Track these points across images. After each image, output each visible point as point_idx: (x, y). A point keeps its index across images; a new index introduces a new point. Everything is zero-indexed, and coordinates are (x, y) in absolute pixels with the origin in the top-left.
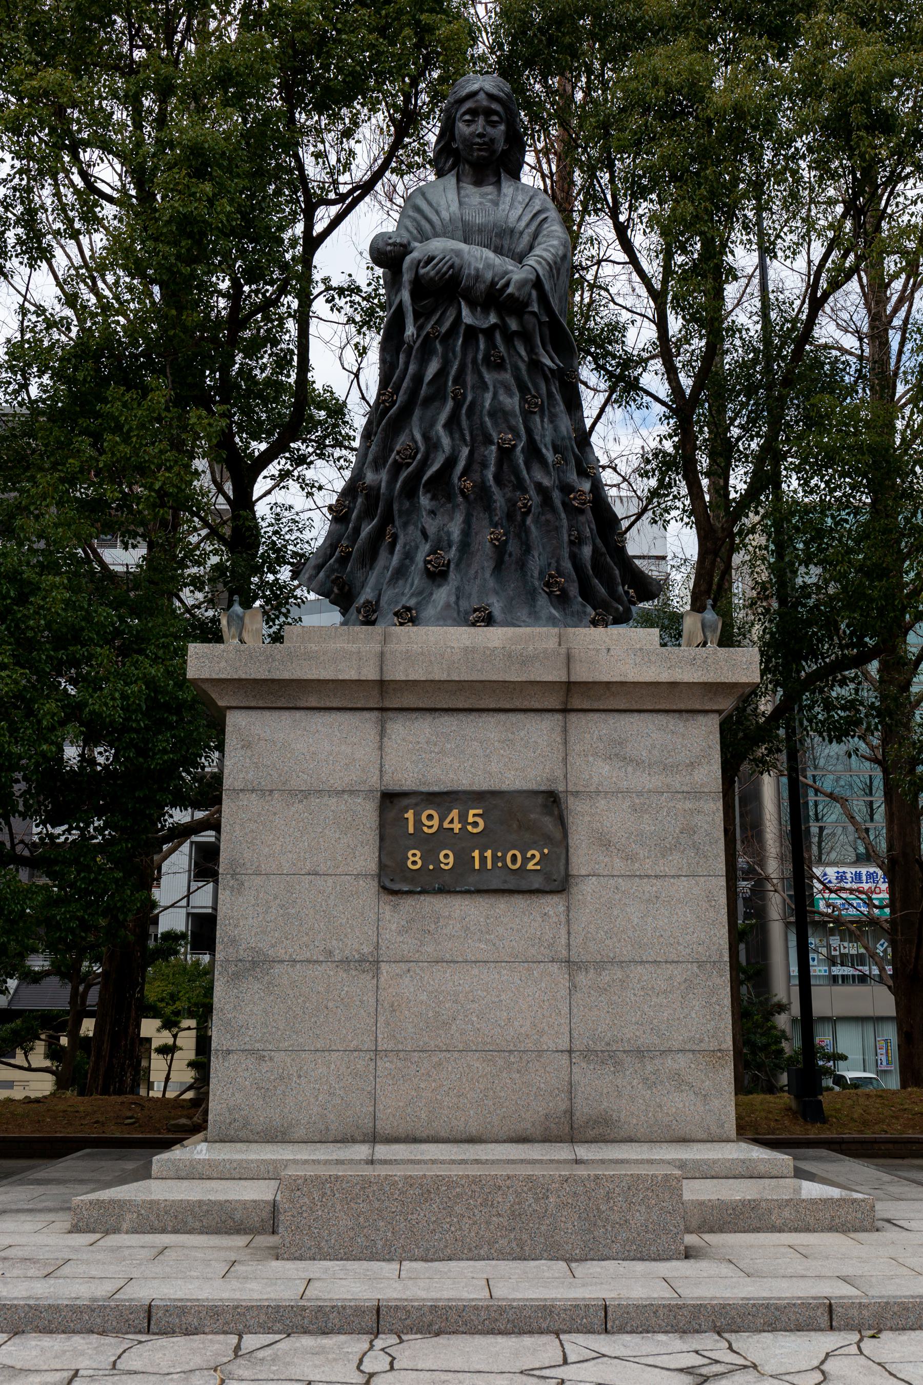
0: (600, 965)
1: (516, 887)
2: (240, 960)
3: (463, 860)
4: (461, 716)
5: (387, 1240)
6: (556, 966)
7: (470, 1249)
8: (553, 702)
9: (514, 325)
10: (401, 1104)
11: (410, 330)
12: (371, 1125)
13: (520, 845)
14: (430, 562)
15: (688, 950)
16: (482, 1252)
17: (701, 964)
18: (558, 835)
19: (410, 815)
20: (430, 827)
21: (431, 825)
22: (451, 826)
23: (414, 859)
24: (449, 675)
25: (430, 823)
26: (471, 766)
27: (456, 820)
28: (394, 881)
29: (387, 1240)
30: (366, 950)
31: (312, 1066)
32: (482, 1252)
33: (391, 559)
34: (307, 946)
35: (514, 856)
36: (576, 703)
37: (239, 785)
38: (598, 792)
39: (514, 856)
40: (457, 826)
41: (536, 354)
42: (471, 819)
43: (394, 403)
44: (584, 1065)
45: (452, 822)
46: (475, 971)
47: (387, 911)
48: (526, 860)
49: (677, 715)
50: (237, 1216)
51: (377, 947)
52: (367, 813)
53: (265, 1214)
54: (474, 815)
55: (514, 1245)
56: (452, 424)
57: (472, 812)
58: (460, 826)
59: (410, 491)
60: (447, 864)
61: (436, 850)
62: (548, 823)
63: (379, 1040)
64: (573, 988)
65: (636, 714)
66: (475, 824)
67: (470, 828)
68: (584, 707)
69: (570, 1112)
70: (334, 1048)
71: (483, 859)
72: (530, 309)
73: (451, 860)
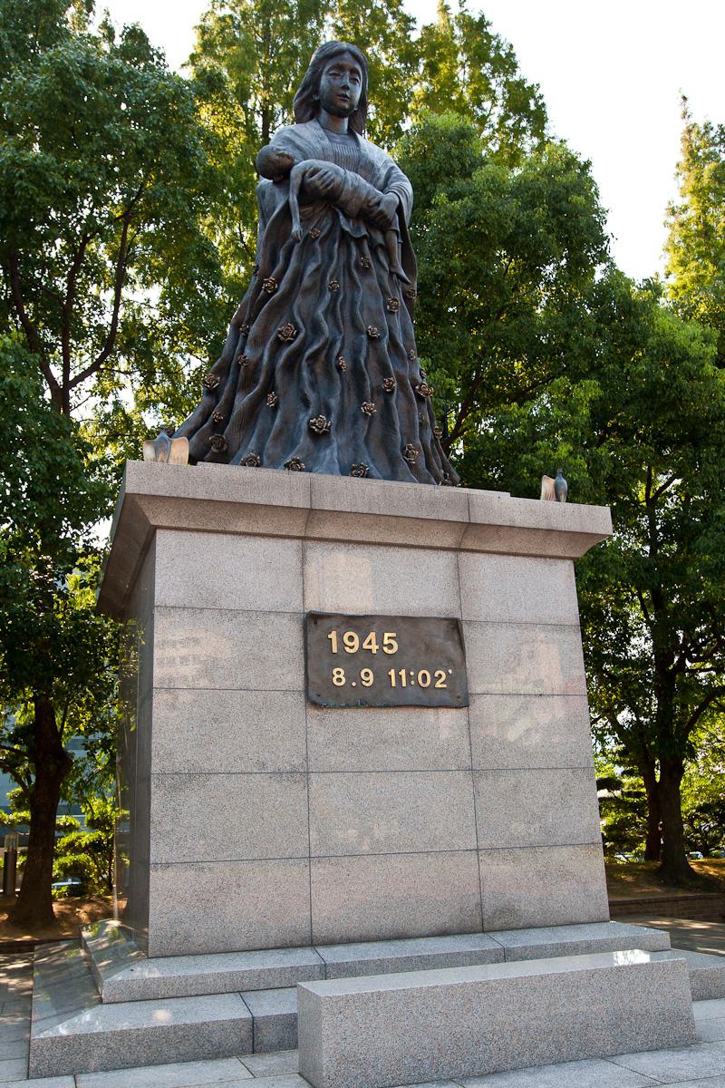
0: (497, 771)
1: (427, 701)
2: (176, 773)
3: (382, 678)
4: (371, 549)
5: (434, 1058)
6: (462, 774)
7: (513, 1057)
8: (448, 541)
9: (379, 239)
10: (335, 907)
11: (296, 228)
12: (308, 929)
13: (422, 664)
14: (314, 424)
15: (564, 759)
16: (525, 1059)
17: (574, 770)
18: (459, 660)
19: (333, 636)
20: (352, 647)
21: (353, 646)
22: (369, 647)
23: (339, 676)
24: (370, 509)
25: (351, 644)
26: (382, 595)
27: (374, 642)
28: (318, 696)
29: (434, 1058)
30: (297, 761)
31: (251, 874)
32: (525, 1059)
33: (273, 421)
34: (241, 758)
35: (424, 675)
36: (469, 544)
37: (170, 602)
38: (487, 622)
39: (424, 675)
40: (374, 648)
41: (395, 267)
42: (386, 642)
43: (275, 291)
44: (489, 861)
45: (370, 643)
46: (394, 780)
47: (314, 725)
48: (435, 679)
49: (543, 560)
50: (215, 1039)
51: (307, 759)
52: (291, 636)
53: (244, 1034)
54: (389, 638)
55: (552, 1047)
56: (331, 311)
57: (387, 635)
58: (377, 647)
59: (292, 364)
60: (368, 682)
61: (361, 670)
62: (451, 647)
63: (312, 847)
64: (476, 793)
65: (512, 557)
66: (390, 646)
67: (385, 649)
68: (474, 548)
69: (480, 905)
70: (271, 857)
71: (399, 678)
72: (394, 228)
73: (371, 678)
